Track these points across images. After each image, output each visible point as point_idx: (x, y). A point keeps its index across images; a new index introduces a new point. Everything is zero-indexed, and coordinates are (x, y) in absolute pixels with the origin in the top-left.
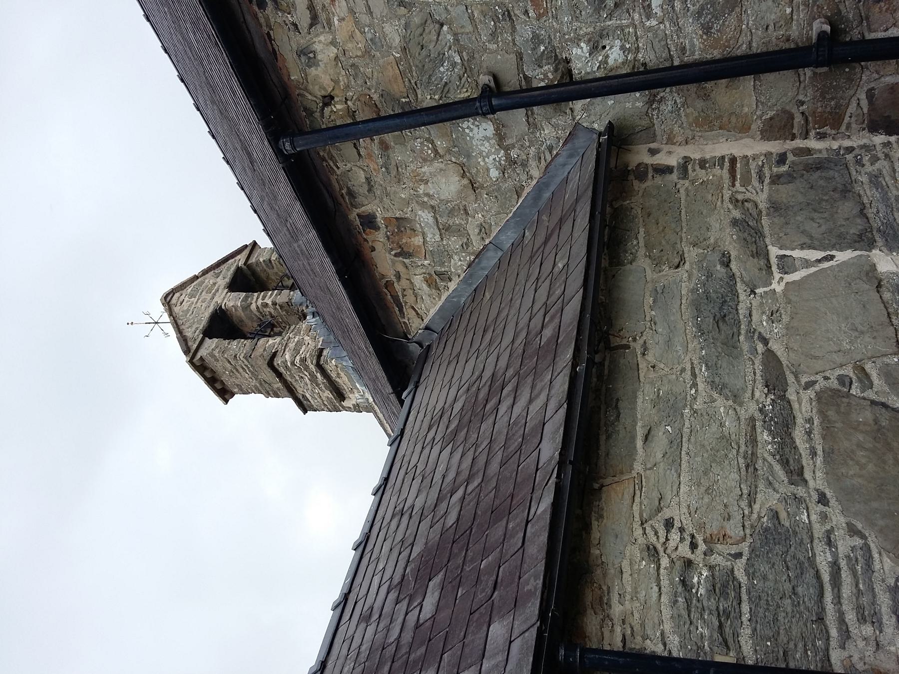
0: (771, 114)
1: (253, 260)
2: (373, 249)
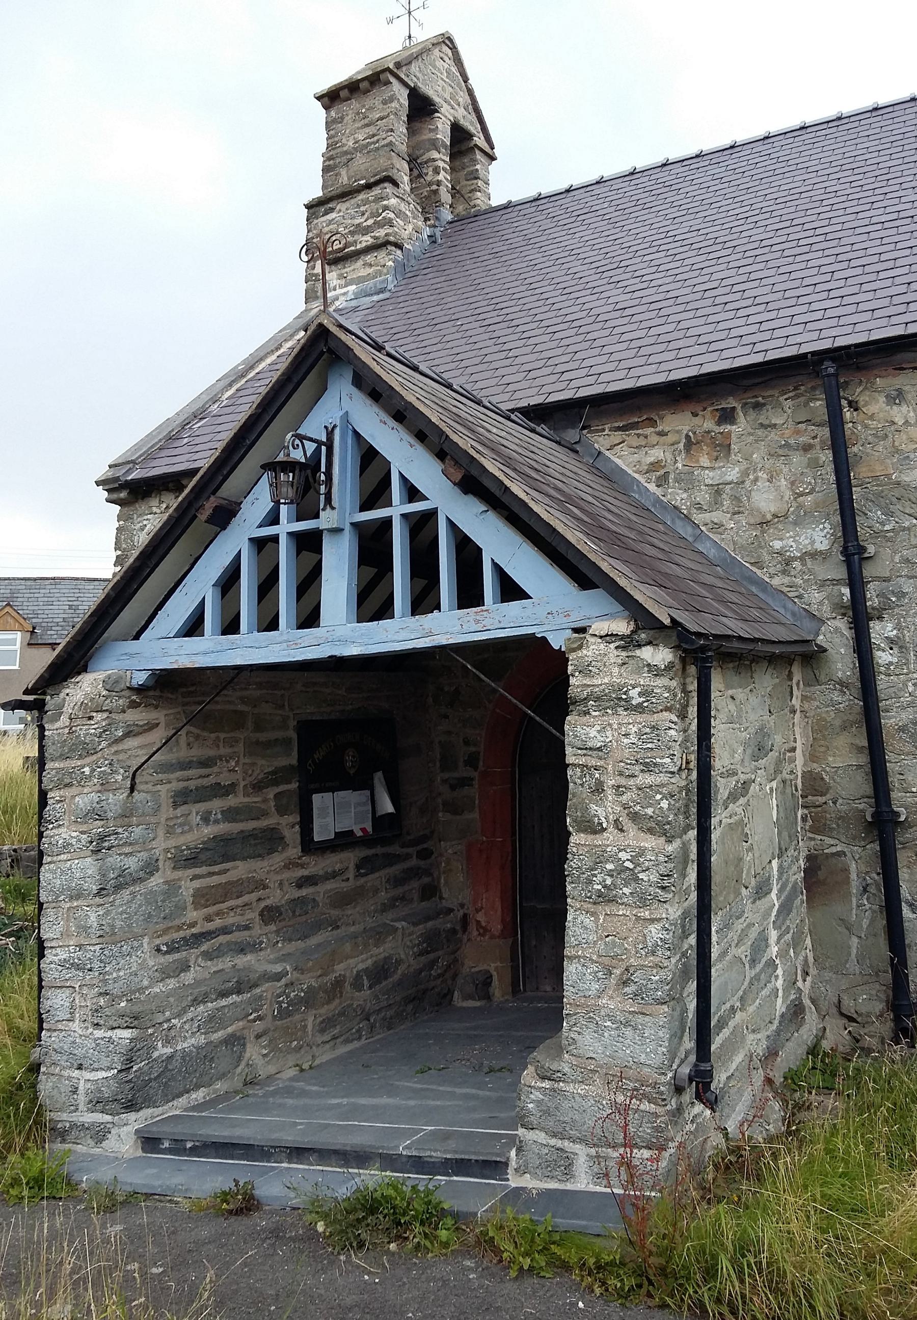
0: (827, 778)
1: (479, 156)
2: (695, 415)
